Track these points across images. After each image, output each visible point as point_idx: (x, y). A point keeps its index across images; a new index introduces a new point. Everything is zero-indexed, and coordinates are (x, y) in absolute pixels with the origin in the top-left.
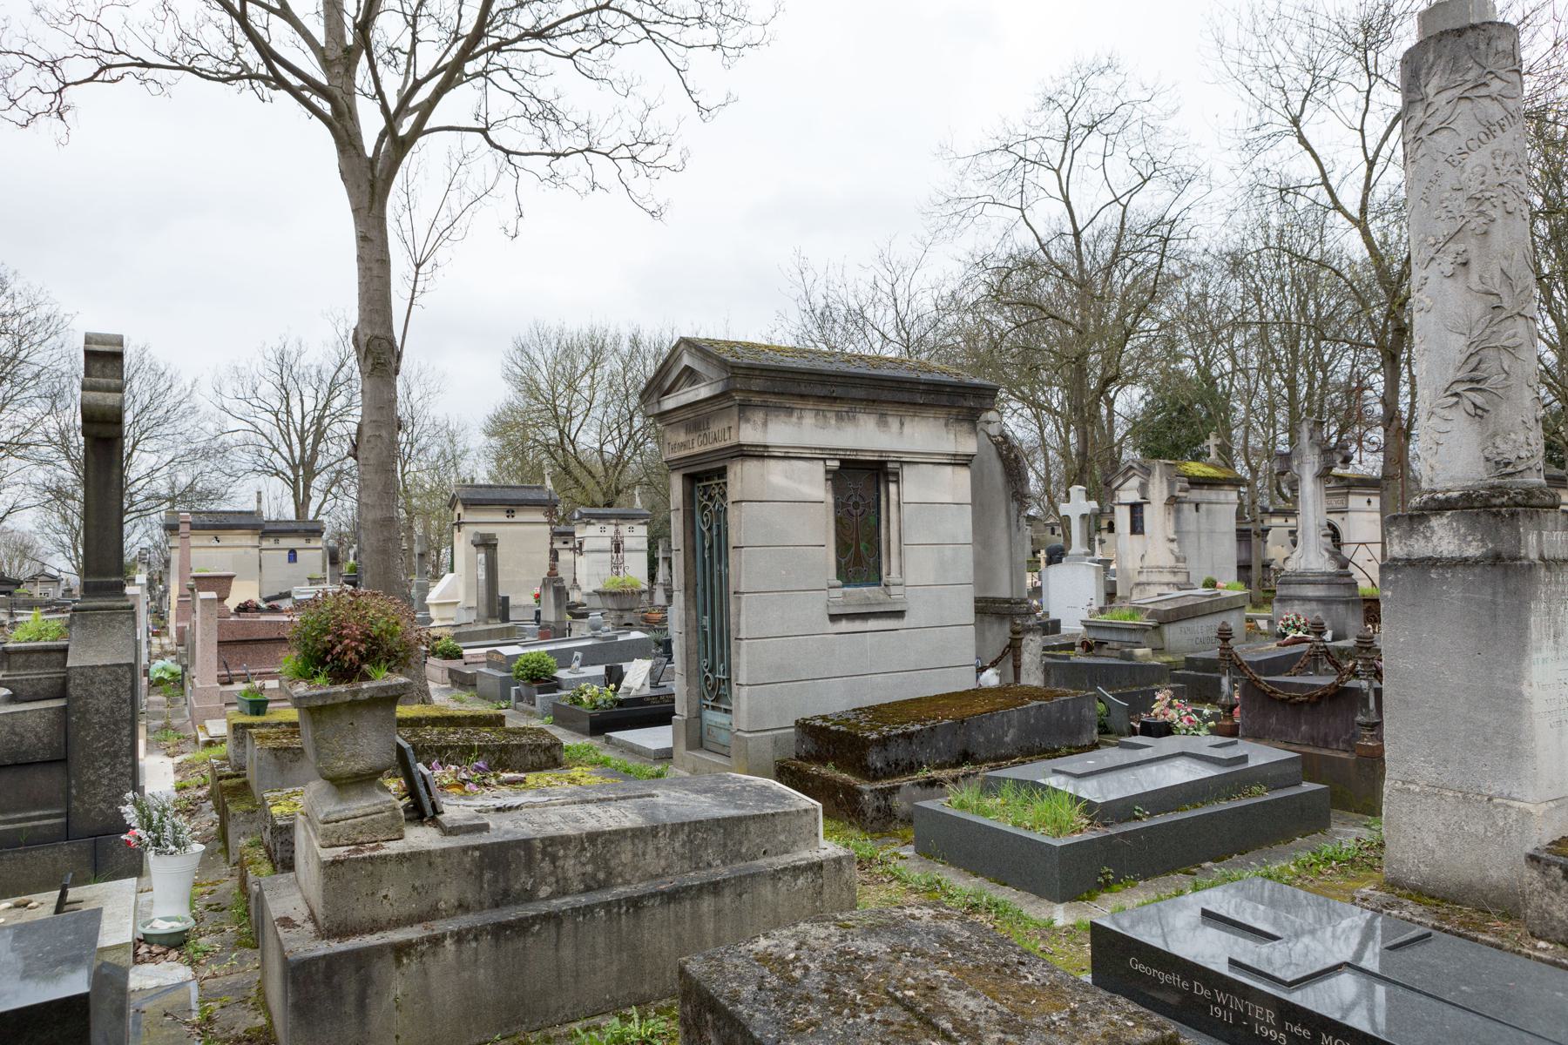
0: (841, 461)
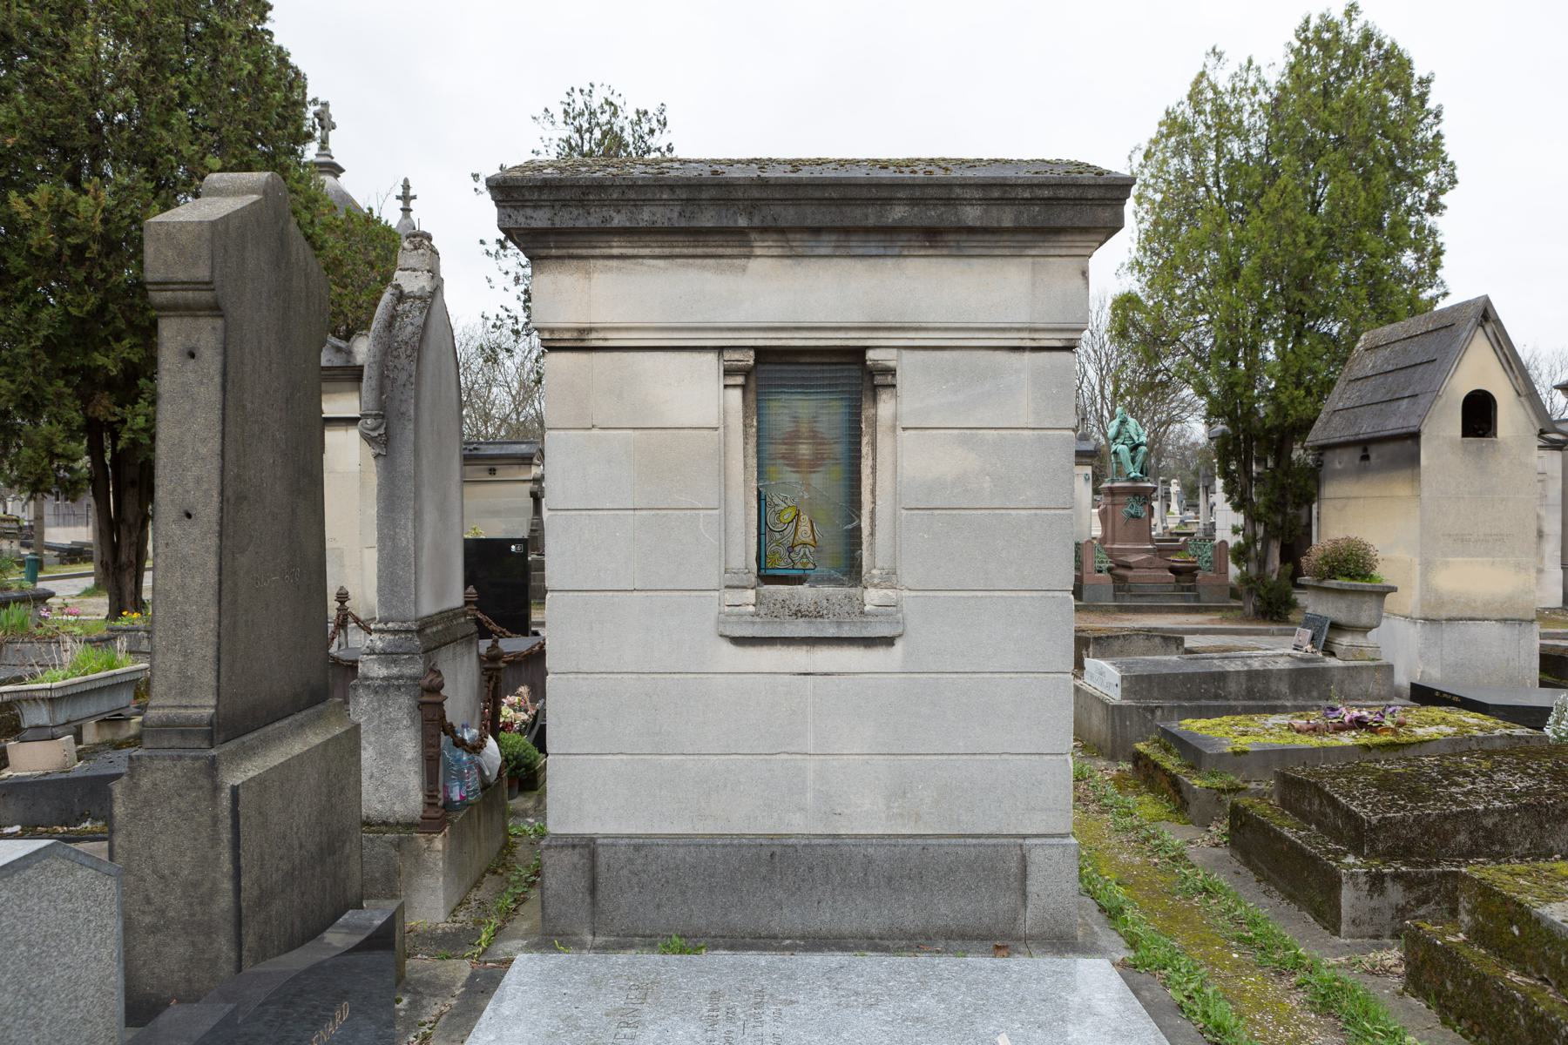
0: (759, 351)
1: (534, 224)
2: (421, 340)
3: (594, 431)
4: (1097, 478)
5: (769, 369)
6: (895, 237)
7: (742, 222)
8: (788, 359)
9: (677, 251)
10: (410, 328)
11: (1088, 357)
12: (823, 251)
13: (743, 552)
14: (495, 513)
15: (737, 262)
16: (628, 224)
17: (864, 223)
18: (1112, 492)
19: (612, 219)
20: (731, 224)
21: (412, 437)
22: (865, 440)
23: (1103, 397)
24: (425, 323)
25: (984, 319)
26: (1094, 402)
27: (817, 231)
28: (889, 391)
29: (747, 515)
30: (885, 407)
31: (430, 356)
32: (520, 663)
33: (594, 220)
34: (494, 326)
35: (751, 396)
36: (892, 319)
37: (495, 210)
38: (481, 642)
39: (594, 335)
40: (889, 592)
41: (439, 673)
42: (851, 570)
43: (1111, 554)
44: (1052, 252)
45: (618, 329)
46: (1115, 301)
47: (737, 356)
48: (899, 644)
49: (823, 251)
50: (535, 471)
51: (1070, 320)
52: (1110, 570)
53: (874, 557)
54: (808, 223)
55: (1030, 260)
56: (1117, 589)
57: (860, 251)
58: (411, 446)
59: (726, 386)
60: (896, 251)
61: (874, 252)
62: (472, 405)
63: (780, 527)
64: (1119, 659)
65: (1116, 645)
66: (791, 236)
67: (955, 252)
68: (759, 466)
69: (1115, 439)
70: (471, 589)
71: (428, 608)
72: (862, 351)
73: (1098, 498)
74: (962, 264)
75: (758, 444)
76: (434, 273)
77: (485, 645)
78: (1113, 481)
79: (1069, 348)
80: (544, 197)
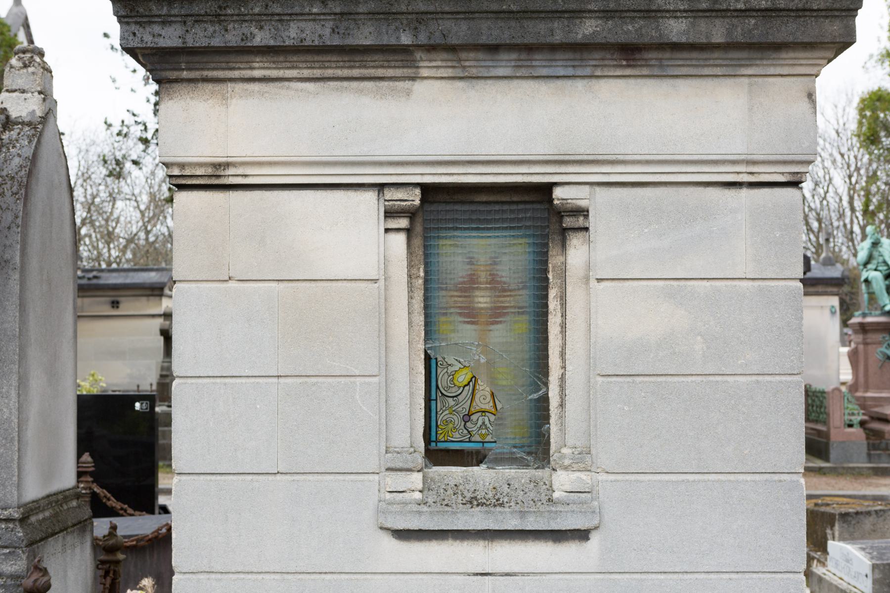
0: (426, 189)
1: (163, 43)
2: (30, 174)
3: (231, 284)
4: (846, 309)
5: (438, 209)
6: (586, 55)
7: (406, 39)
8: (459, 197)
9: (329, 72)
10: (17, 161)
11: (834, 162)
12: (501, 72)
13: (409, 428)
14: (118, 354)
15: (400, 84)
16: (272, 43)
17: (549, 40)
18: (863, 328)
19: (253, 36)
20: (393, 41)
21: (17, 288)
22: (552, 293)
23: (853, 210)
24: (35, 155)
25: (692, 150)
26: (841, 216)
27: (493, 49)
28: (581, 234)
29: (412, 382)
30: (575, 254)
31: (40, 193)
32: (143, 548)
33: (233, 38)
34: (119, 134)
35: (418, 242)
36: (583, 150)
37: (118, 26)
38: (97, 522)
39: (231, 171)
40: (583, 476)
41: (45, 572)
42: (537, 449)
43: (863, 404)
44: (772, 71)
45: (260, 164)
46: (863, 100)
47: (399, 194)
48: (595, 537)
49: (501, 72)
50: (166, 304)
51: (795, 150)
52: (862, 424)
53: (564, 433)
54: (483, 40)
55: (746, 80)
56: (872, 447)
57: (544, 72)
58: (15, 299)
59: (387, 230)
60: (588, 71)
61: (562, 72)
62: (92, 223)
63: (454, 391)
64: (869, 543)
65: (868, 523)
66: (463, 55)
67: (656, 72)
68: (427, 324)
69: (866, 264)
70: (86, 457)
71: (33, 491)
72: (547, 189)
73: (846, 330)
74: (665, 86)
75: (426, 299)
76: (46, 94)
77: (101, 526)
78: (864, 315)
79: (795, 184)
80: (175, 11)
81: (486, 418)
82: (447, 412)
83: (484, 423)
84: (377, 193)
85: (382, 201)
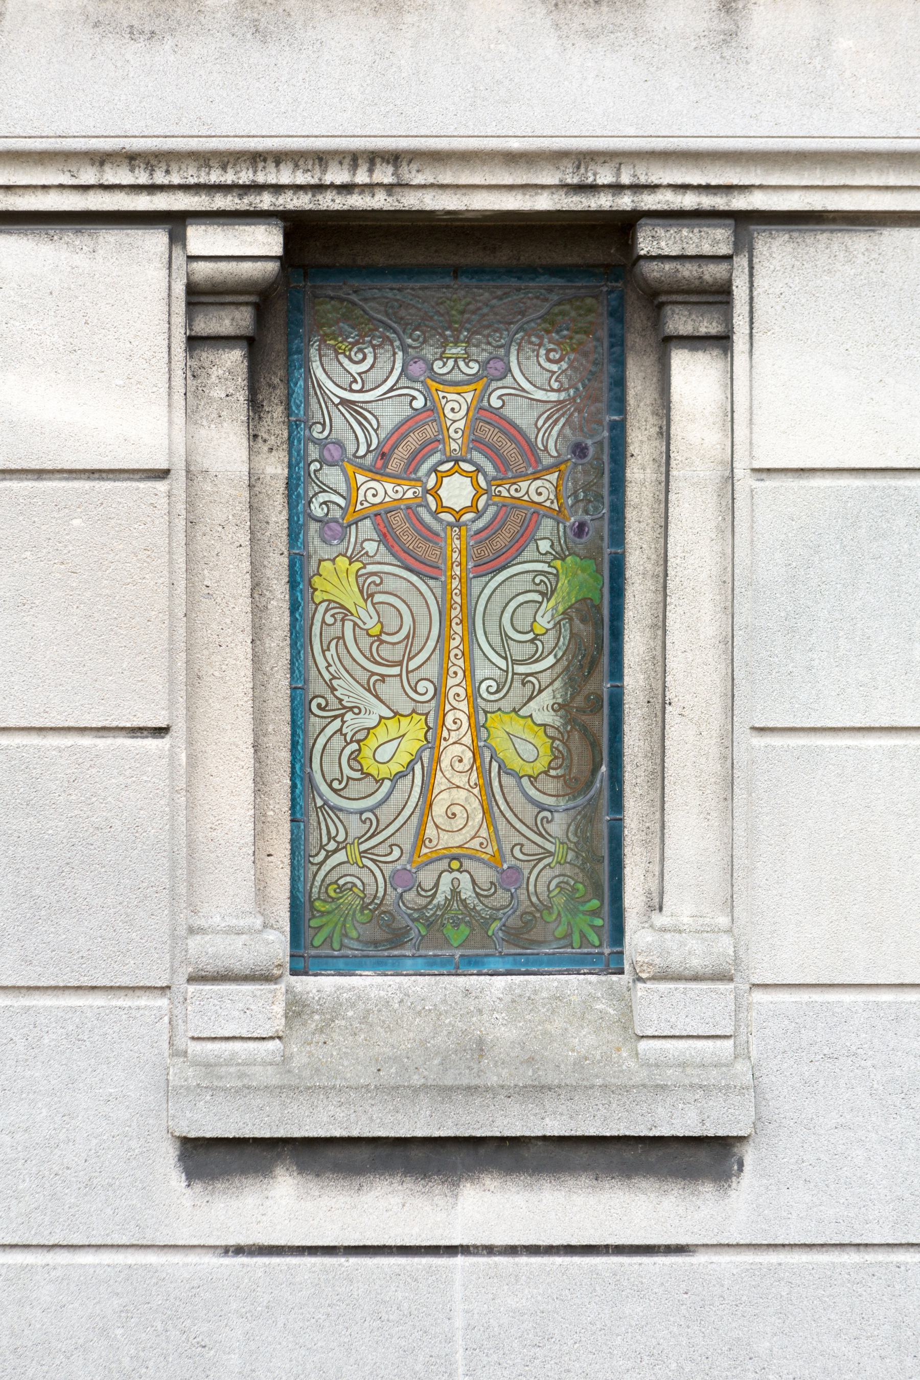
72: (624, 225)
81: (465, 878)
82: (340, 856)
83: (455, 892)
84: (166, 239)
85: (179, 259)
